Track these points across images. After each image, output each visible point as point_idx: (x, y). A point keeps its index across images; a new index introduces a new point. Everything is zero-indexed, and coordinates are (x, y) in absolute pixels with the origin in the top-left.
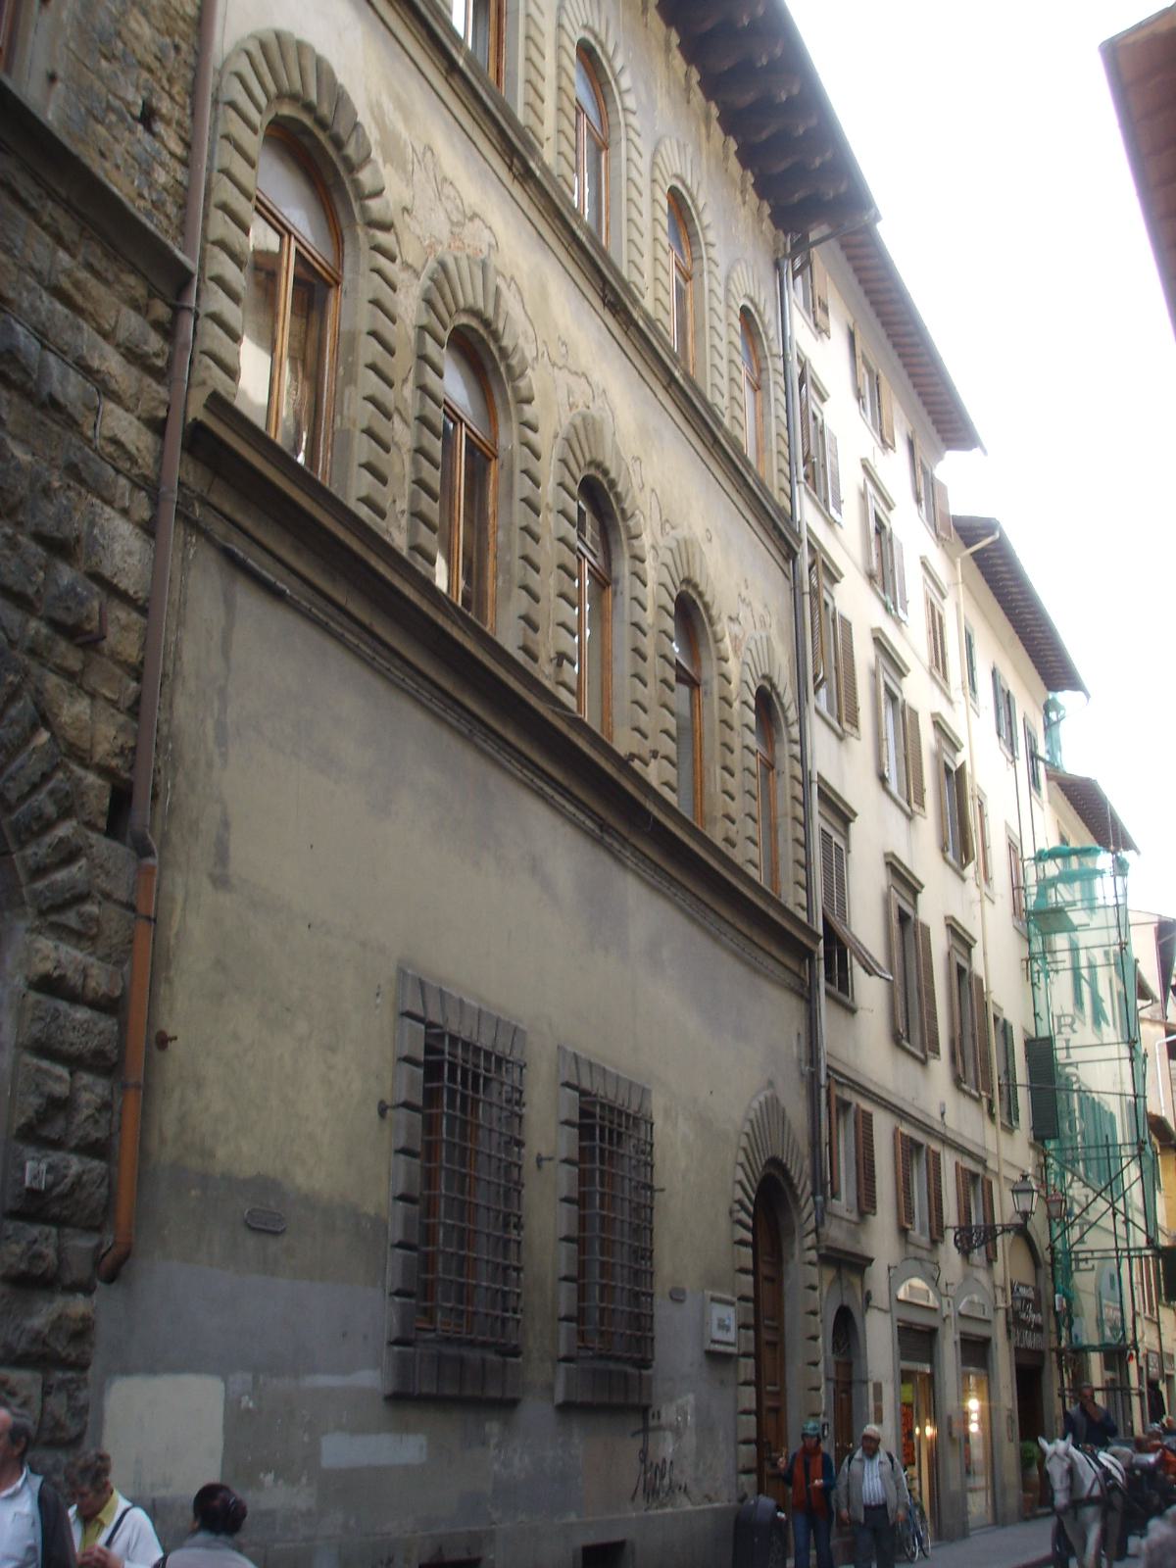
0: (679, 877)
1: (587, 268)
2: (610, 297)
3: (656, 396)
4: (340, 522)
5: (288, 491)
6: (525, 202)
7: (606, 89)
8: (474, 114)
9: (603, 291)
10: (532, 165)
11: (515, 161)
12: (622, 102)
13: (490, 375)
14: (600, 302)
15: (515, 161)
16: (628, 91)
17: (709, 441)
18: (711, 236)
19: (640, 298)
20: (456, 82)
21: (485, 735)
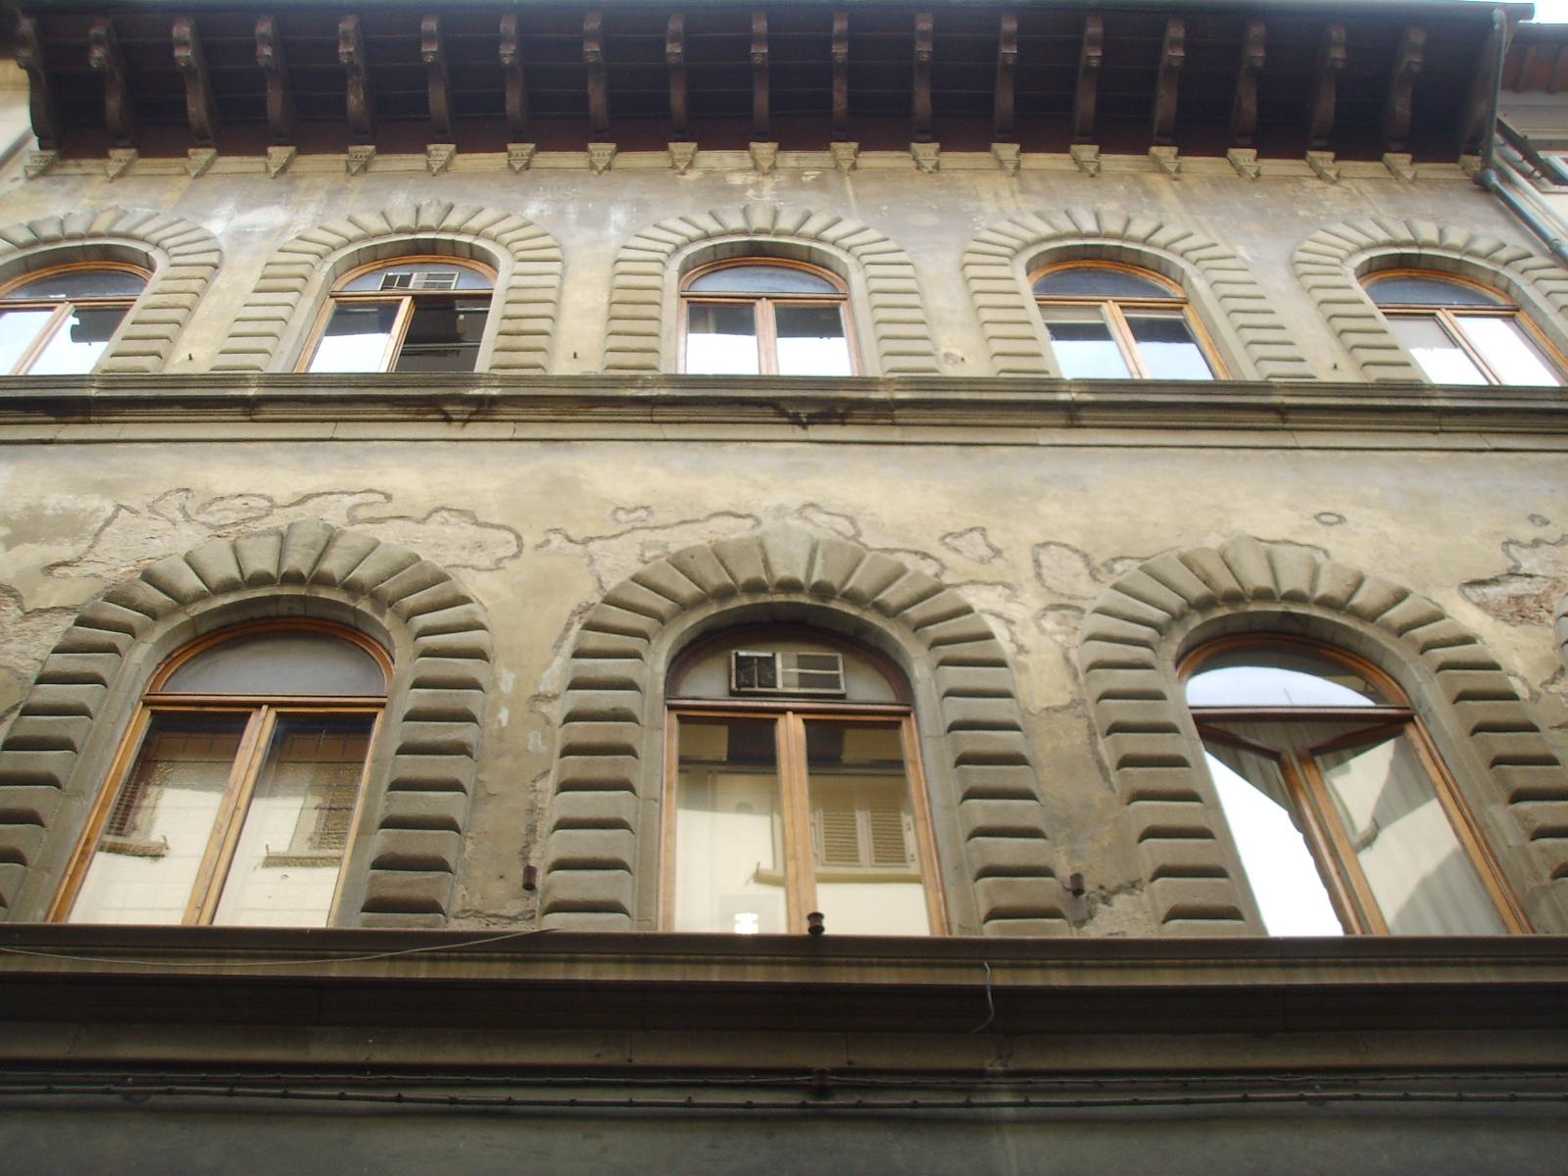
0: (1301, 1060)
1: (719, 412)
2: (803, 412)
3: (1037, 445)
4: (1468, 964)
5: (464, 975)
6: (504, 431)
7: (816, 257)
8: (17, 419)
9: (783, 414)
10: (1063, 397)
11: (449, 408)
12: (1134, 240)
13: (361, 626)
14: (798, 428)
15: (449, 408)
16: (1441, 232)
17: (1270, 419)
18: (1456, 236)
19: (1046, 376)
20: (268, 411)
21: (162, 1082)
